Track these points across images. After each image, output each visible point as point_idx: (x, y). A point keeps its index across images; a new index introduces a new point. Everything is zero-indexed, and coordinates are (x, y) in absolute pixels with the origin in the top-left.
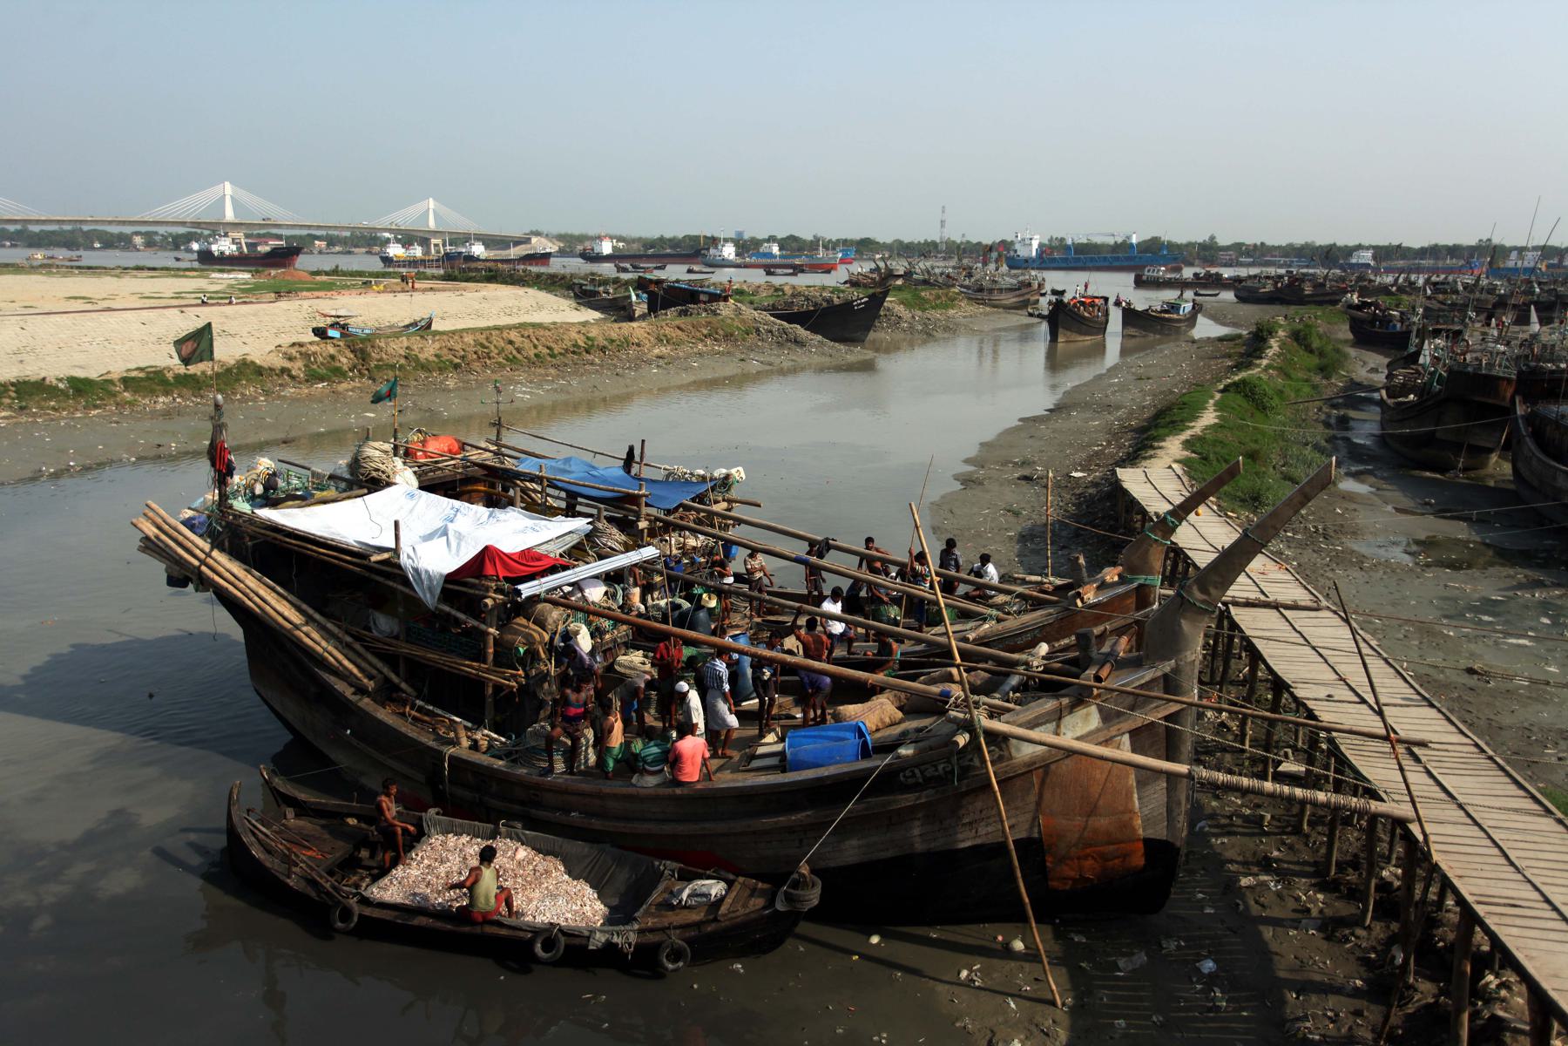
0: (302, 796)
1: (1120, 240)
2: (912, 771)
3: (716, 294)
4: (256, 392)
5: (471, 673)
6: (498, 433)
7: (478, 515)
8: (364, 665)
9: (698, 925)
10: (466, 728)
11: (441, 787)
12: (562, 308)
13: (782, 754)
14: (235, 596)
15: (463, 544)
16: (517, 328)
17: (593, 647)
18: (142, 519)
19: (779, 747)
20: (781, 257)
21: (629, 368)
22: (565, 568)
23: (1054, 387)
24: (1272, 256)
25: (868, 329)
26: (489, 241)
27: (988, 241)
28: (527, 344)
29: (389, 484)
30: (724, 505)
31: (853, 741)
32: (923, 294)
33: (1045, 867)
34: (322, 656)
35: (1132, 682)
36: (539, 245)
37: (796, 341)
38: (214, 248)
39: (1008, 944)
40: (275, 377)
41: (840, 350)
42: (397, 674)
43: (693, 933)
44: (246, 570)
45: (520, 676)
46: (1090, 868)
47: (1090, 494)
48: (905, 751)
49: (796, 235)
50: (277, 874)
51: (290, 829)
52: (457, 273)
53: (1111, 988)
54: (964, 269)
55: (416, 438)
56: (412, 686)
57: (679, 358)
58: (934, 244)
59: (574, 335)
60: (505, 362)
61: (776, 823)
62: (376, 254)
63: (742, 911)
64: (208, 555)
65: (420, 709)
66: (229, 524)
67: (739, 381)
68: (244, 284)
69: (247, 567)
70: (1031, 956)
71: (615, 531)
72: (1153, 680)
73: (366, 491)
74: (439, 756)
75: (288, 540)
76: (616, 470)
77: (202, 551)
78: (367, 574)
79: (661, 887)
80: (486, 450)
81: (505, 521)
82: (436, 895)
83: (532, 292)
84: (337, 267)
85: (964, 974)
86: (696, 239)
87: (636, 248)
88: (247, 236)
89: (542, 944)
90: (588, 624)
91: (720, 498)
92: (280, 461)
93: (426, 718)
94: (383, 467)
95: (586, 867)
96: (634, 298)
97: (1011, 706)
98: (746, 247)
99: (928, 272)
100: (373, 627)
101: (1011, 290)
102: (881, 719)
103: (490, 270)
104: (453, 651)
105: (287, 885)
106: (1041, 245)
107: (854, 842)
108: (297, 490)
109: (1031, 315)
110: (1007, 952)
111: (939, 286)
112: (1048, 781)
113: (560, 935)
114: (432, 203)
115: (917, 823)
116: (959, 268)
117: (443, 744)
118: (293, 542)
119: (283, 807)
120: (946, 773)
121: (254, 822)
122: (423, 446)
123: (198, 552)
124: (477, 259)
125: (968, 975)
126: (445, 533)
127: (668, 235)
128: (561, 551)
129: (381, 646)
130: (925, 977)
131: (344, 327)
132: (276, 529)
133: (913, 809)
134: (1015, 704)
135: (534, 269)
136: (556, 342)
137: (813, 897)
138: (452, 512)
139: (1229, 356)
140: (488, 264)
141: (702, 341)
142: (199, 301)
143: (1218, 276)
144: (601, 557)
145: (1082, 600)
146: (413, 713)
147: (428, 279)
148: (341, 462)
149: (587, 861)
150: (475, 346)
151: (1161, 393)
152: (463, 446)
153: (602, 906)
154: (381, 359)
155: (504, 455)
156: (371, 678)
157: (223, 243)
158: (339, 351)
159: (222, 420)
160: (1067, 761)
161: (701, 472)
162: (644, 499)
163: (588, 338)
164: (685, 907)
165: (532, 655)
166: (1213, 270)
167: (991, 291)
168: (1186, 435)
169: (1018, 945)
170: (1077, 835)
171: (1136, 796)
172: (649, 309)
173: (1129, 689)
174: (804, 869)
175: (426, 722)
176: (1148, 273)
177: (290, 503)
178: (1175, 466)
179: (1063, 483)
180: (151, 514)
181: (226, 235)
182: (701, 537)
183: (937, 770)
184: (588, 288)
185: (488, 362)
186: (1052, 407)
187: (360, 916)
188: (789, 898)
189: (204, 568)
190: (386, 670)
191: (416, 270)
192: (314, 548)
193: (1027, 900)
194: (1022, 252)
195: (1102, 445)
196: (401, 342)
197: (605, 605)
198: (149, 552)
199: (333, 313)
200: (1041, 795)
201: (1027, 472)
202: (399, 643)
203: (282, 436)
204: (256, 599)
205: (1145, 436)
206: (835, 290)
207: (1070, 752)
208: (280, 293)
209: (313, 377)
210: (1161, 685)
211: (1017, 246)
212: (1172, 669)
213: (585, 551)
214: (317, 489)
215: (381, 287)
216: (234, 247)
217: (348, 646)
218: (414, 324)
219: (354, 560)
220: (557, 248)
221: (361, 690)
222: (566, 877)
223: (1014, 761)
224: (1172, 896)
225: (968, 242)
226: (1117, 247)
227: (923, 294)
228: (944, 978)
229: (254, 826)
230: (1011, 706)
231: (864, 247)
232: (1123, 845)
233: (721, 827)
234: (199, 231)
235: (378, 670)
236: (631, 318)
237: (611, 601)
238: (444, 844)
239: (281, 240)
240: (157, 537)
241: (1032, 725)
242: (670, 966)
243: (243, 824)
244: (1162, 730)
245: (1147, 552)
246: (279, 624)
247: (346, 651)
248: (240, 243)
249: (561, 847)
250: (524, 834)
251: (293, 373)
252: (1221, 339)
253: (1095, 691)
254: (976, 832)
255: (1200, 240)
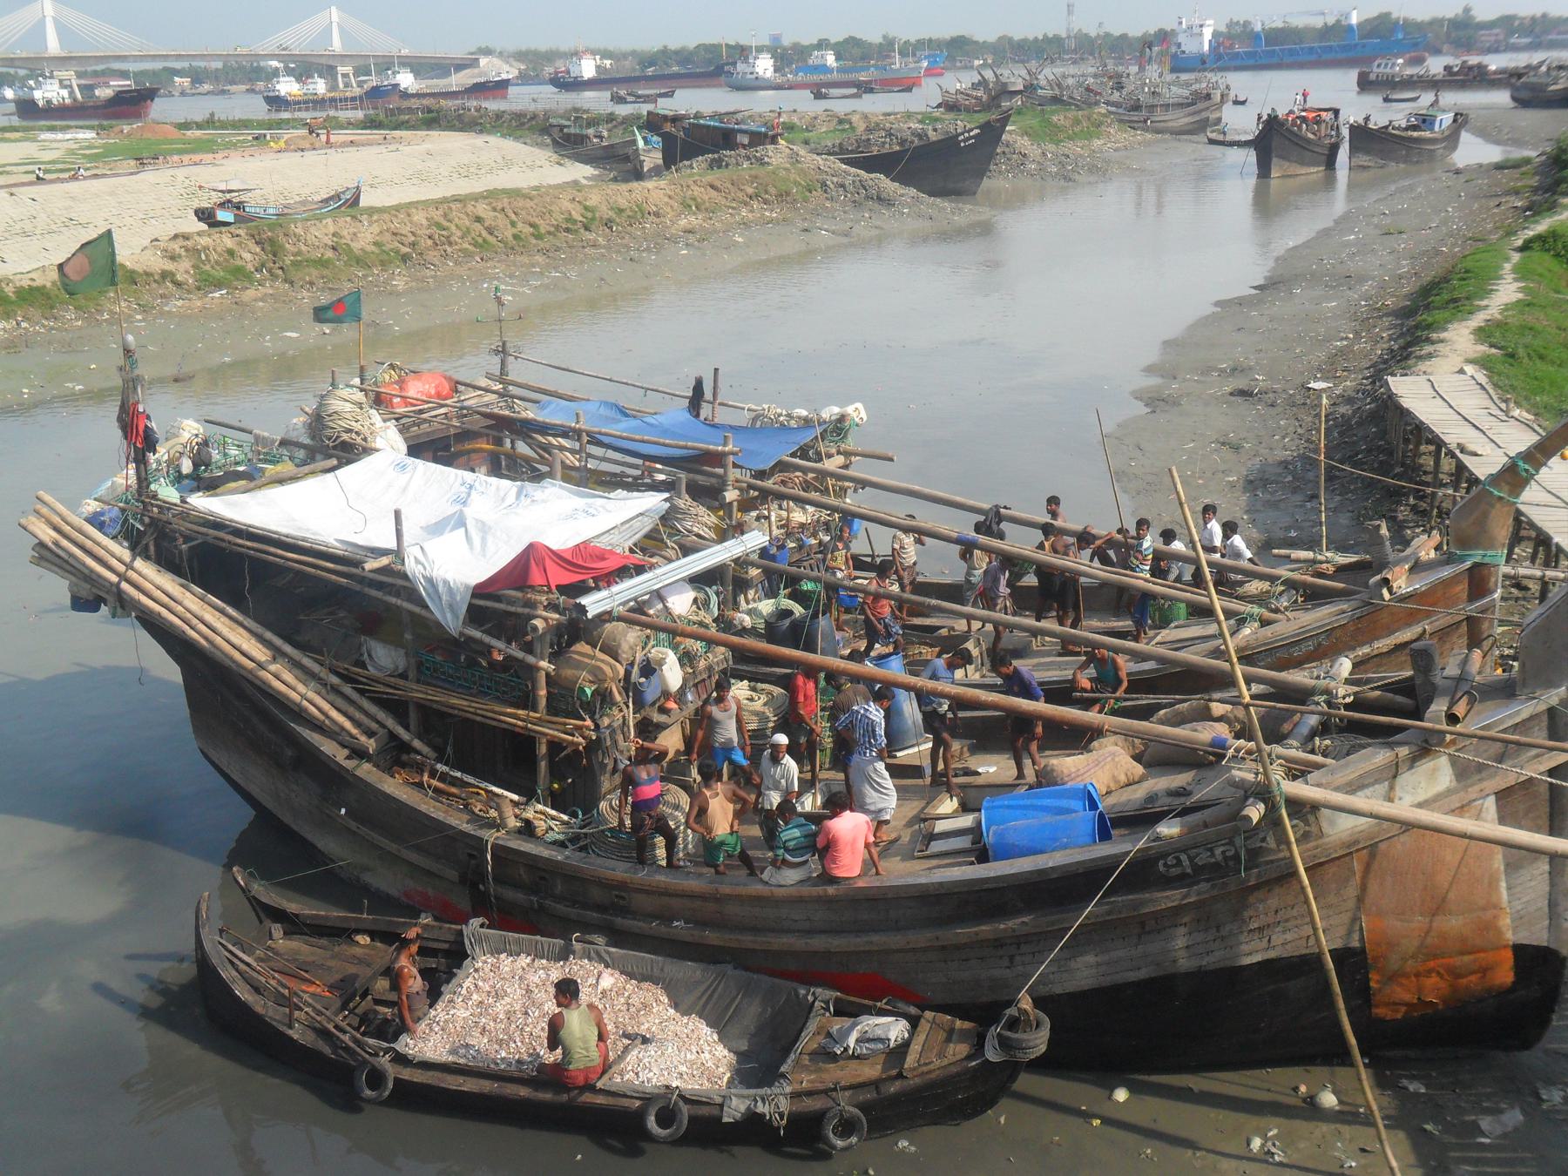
0: (292, 906)
1: (1331, 20)
2: (1178, 859)
3: (759, 134)
4: (129, 307)
5: (515, 725)
6: (503, 363)
7: (502, 494)
8: (358, 715)
9: (875, 1084)
10: (515, 804)
11: (481, 887)
12: (539, 163)
13: (976, 831)
14: (171, 624)
15: (490, 539)
16: (485, 198)
17: (685, 680)
18: (33, 519)
19: (967, 821)
20: (839, 70)
21: (648, 249)
22: (640, 570)
23: (1265, 245)
24: (1559, 34)
25: (981, 173)
26: (419, 66)
27: (1135, 31)
28: (501, 222)
29: (367, 451)
30: (840, 460)
31: (1084, 820)
32: (1055, 118)
33: (1368, 988)
34: (299, 705)
35: (1501, 721)
36: (492, 68)
37: (879, 198)
38: (38, 95)
39: (1312, 1097)
40: (154, 285)
41: (944, 209)
42: (407, 728)
43: (868, 1095)
44: (182, 586)
45: (588, 728)
46: (1434, 989)
47: (1343, 416)
48: (1169, 829)
49: (858, 36)
50: (274, 1023)
51: (277, 953)
52: (382, 116)
53: (1477, 1162)
54: (1110, 78)
55: (387, 377)
56: (429, 744)
57: (716, 231)
58: (1056, 41)
59: (567, 205)
60: (471, 248)
61: (976, 934)
62: (260, 92)
63: (937, 1063)
64: (129, 566)
65: (443, 778)
66: (154, 522)
67: (805, 258)
68: (88, 148)
69: (183, 581)
70: (1349, 1116)
71: (702, 510)
72: (1531, 718)
73: (334, 462)
74: (480, 844)
75: (240, 541)
76: (675, 413)
77: (120, 560)
78: (358, 587)
79: (812, 1026)
80: (487, 390)
81: (544, 501)
82: (496, 1047)
83: (494, 140)
84: (212, 115)
85: (1256, 1143)
86: (713, 49)
87: (629, 67)
88: (79, 75)
89: (656, 1116)
90: (675, 647)
91: (834, 451)
92: (207, 421)
93: (454, 790)
94: (356, 426)
95: (700, 998)
96: (641, 143)
97: (1319, 759)
98: (786, 57)
99: (1059, 85)
100: (368, 661)
101: (1181, 105)
102: (1114, 777)
103: (430, 111)
104: (486, 694)
105: (291, 1039)
106: (1216, 34)
107: (1090, 959)
108: (237, 463)
109: (1212, 142)
110: (1311, 1109)
111: (1076, 106)
112: (1375, 866)
113: (681, 1103)
114: (335, 14)
115: (1182, 930)
116: (1103, 76)
117: (481, 827)
118: (249, 544)
119: (268, 923)
120: (1226, 859)
121: (230, 947)
122: (401, 389)
123: (114, 563)
124: (405, 95)
125: (1263, 1145)
126: (461, 522)
127: (673, 45)
128: (630, 543)
129: (382, 688)
130: (1200, 1149)
131: (239, 206)
132: (219, 525)
133: (1177, 911)
134: (1325, 756)
135: (493, 105)
136: (542, 215)
137: (1038, 1041)
138: (463, 489)
139: (1516, 192)
140: (426, 102)
141: (746, 204)
142: (32, 177)
143: (1481, 68)
144: (686, 551)
145: (1391, 592)
146: (435, 783)
147: (342, 128)
148: (295, 421)
149: (702, 988)
150: (429, 227)
151: (1424, 253)
152: (456, 386)
153: (726, 1052)
154: (299, 253)
155: (513, 397)
156: (370, 734)
157: (49, 87)
158: (240, 244)
159: (137, 372)
160: (1403, 838)
161: (804, 413)
162: (731, 458)
163: (586, 208)
164: (854, 1057)
165: (604, 697)
166: (1473, 60)
167: (1152, 108)
168: (1478, 320)
169: (1329, 1099)
170: (1416, 943)
171: (1503, 884)
172: (664, 158)
173: (1492, 733)
174: (1026, 1003)
175: (453, 795)
176: (1378, 70)
177: (233, 485)
178: (1469, 369)
179: (1299, 399)
180: (45, 510)
181: (52, 77)
182: (810, 509)
183: (1213, 855)
184: (572, 131)
185: (449, 250)
186: (1262, 282)
187: (396, 1079)
188: (1004, 1043)
189: (124, 585)
190: (390, 723)
191: (324, 114)
192: (280, 552)
193: (1353, 1041)
194: (1189, 47)
195: (1347, 338)
196: (325, 226)
197: (695, 618)
198: (45, 564)
199: (223, 187)
200: (1364, 888)
201: (1242, 383)
202: (407, 684)
203: (171, 371)
204: (201, 627)
205: (1411, 322)
206: (925, 118)
207: (1408, 826)
208: (145, 158)
209: (207, 283)
210: (1545, 723)
211: (1181, 38)
212: (1561, 701)
213: (662, 541)
214: (266, 461)
215: (282, 144)
216: (65, 93)
217: (335, 690)
218: (337, 197)
219: (339, 568)
220: (516, 73)
221: (358, 753)
222: (672, 1011)
223: (1326, 840)
224: (1554, 1023)
225: (1107, 35)
226: (1327, 32)
227: (1055, 118)
228: (1227, 1150)
229: (230, 952)
230: (1319, 759)
231: (957, 49)
232: (1482, 955)
233: (895, 940)
234: (12, 71)
235: (378, 722)
236: (638, 175)
237: (702, 613)
238: (495, 968)
239: (129, 79)
240: (56, 544)
241: (1353, 788)
242: (839, 1143)
243: (218, 952)
244: (1544, 791)
245: (1485, 515)
246: (234, 661)
247: (332, 697)
248: (71, 86)
249: (662, 970)
250: (608, 952)
251: (179, 278)
252: (1499, 167)
253: (1448, 737)
254: (1269, 941)
255: (1450, 14)
